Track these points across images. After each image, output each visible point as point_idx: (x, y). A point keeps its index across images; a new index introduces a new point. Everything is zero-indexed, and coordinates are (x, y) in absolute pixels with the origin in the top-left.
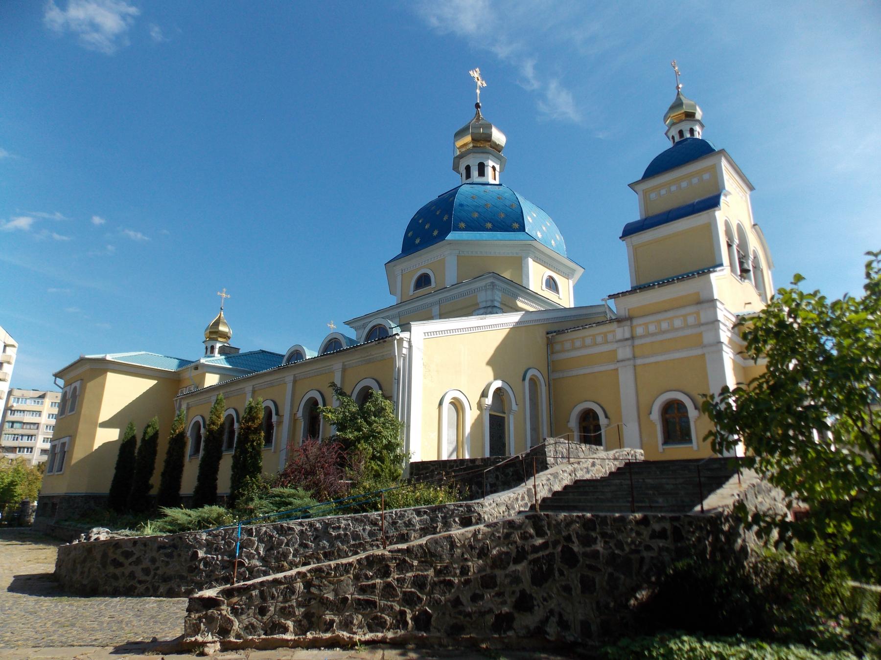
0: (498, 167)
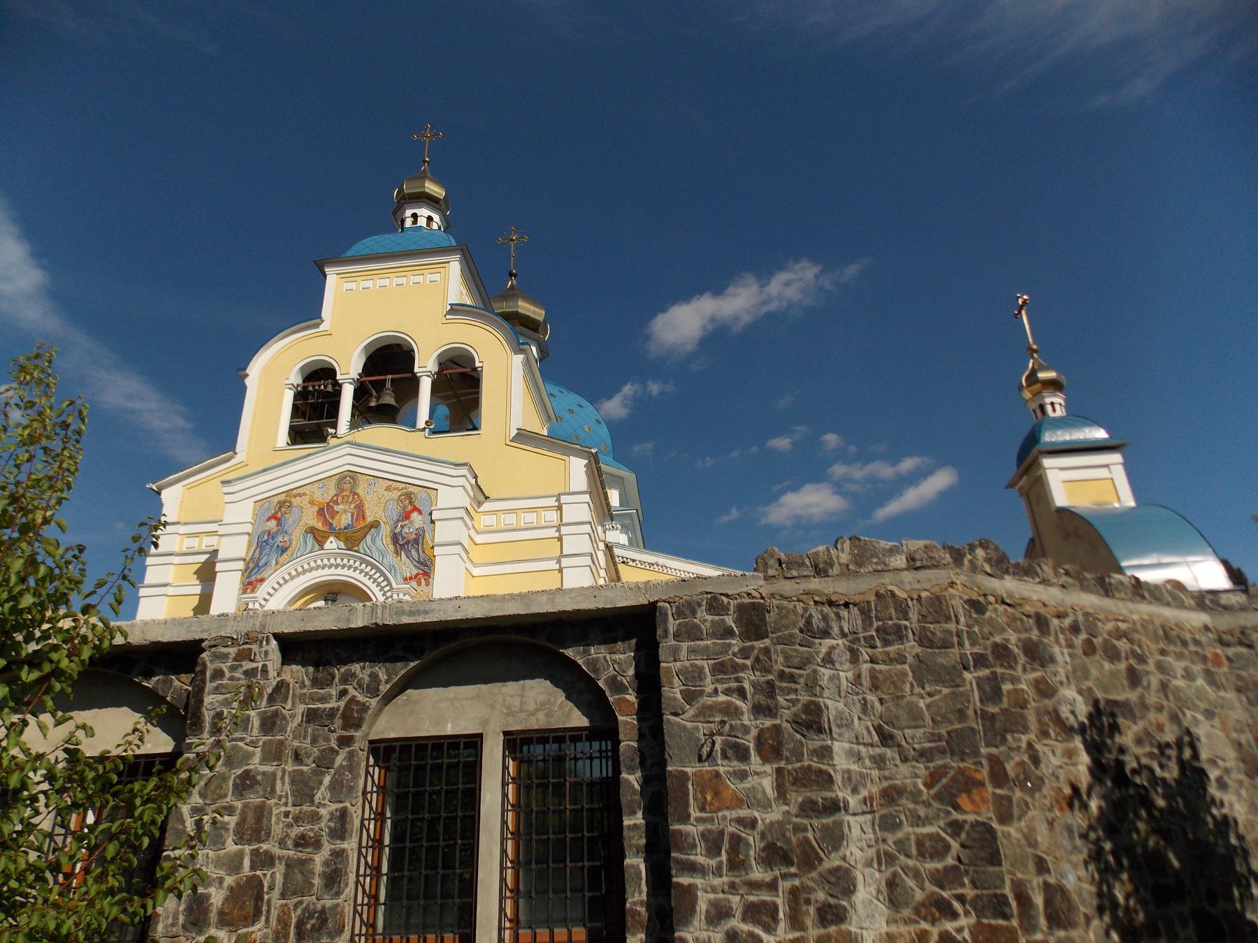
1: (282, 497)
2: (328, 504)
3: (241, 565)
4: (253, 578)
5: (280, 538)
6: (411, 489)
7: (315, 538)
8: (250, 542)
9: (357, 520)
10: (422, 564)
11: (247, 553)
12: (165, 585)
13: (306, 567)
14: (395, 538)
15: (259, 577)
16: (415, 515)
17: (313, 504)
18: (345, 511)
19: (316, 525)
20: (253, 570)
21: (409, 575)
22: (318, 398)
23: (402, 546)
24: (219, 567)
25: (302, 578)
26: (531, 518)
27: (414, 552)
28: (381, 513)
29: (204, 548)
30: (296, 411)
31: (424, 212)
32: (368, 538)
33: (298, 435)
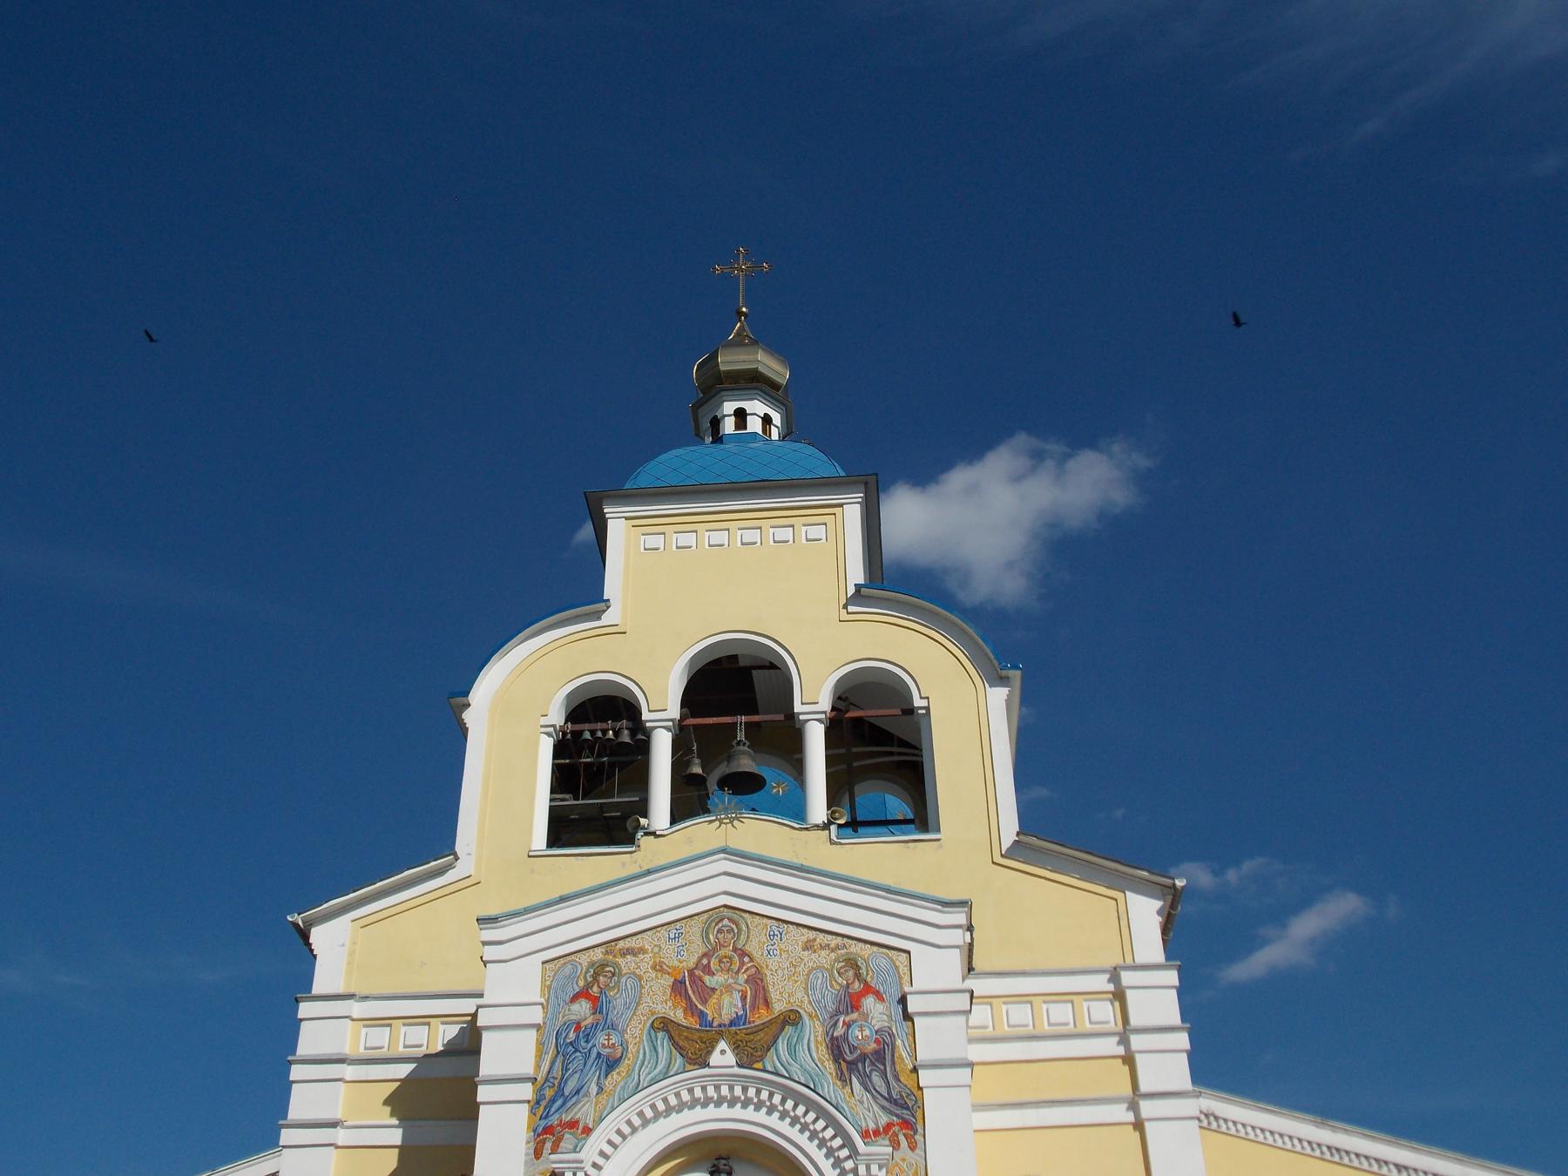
0: (776, 418)
1: (598, 955)
2: (691, 972)
3: (527, 1091)
4: (554, 1120)
5: (601, 1038)
6: (856, 948)
7: (671, 1038)
8: (541, 1045)
9: (754, 1007)
10: (896, 1103)
11: (538, 1066)
12: (334, 1124)
13: (686, 1096)
14: (837, 1048)
15: (566, 1118)
16: (869, 1002)
17: (662, 970)
18: (728, 988)
19: (671, 1015)
20: (553, 1101)
21: (872, 1126)
22: (599, 756)
23: (852, 1065)
24: (483, 1093)
25: (676, 1120)
26: (1061, 1013)
27: (876, 1079)
28: (800, 994)
29: (401, 1049)
30: (563, 779)
31: (757, 407)
32: (782, 1045)
33: (563, 831)
